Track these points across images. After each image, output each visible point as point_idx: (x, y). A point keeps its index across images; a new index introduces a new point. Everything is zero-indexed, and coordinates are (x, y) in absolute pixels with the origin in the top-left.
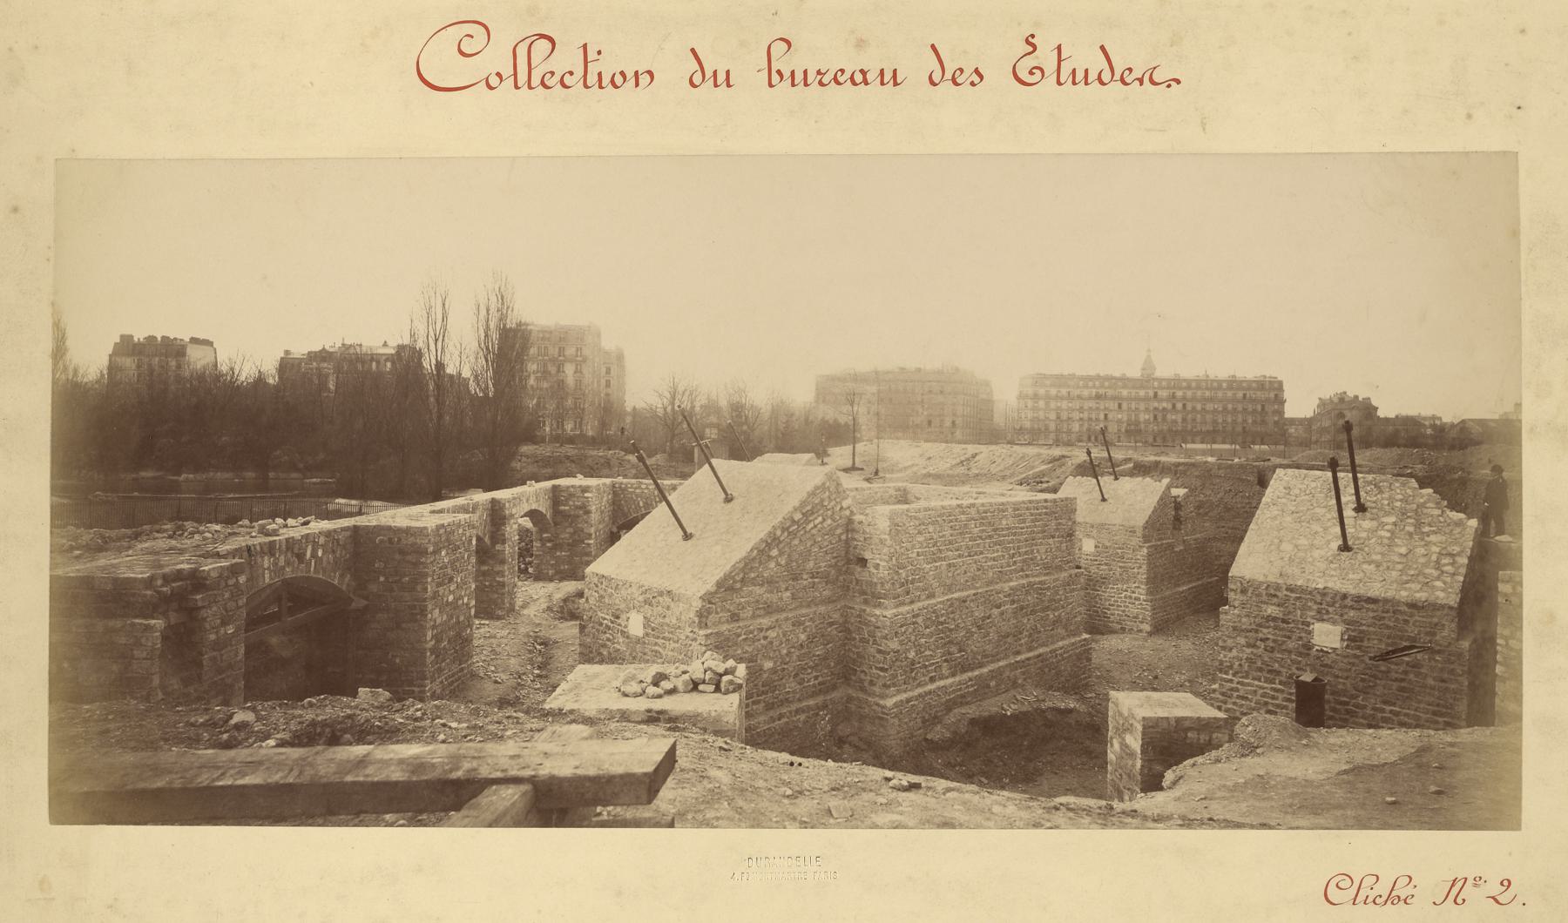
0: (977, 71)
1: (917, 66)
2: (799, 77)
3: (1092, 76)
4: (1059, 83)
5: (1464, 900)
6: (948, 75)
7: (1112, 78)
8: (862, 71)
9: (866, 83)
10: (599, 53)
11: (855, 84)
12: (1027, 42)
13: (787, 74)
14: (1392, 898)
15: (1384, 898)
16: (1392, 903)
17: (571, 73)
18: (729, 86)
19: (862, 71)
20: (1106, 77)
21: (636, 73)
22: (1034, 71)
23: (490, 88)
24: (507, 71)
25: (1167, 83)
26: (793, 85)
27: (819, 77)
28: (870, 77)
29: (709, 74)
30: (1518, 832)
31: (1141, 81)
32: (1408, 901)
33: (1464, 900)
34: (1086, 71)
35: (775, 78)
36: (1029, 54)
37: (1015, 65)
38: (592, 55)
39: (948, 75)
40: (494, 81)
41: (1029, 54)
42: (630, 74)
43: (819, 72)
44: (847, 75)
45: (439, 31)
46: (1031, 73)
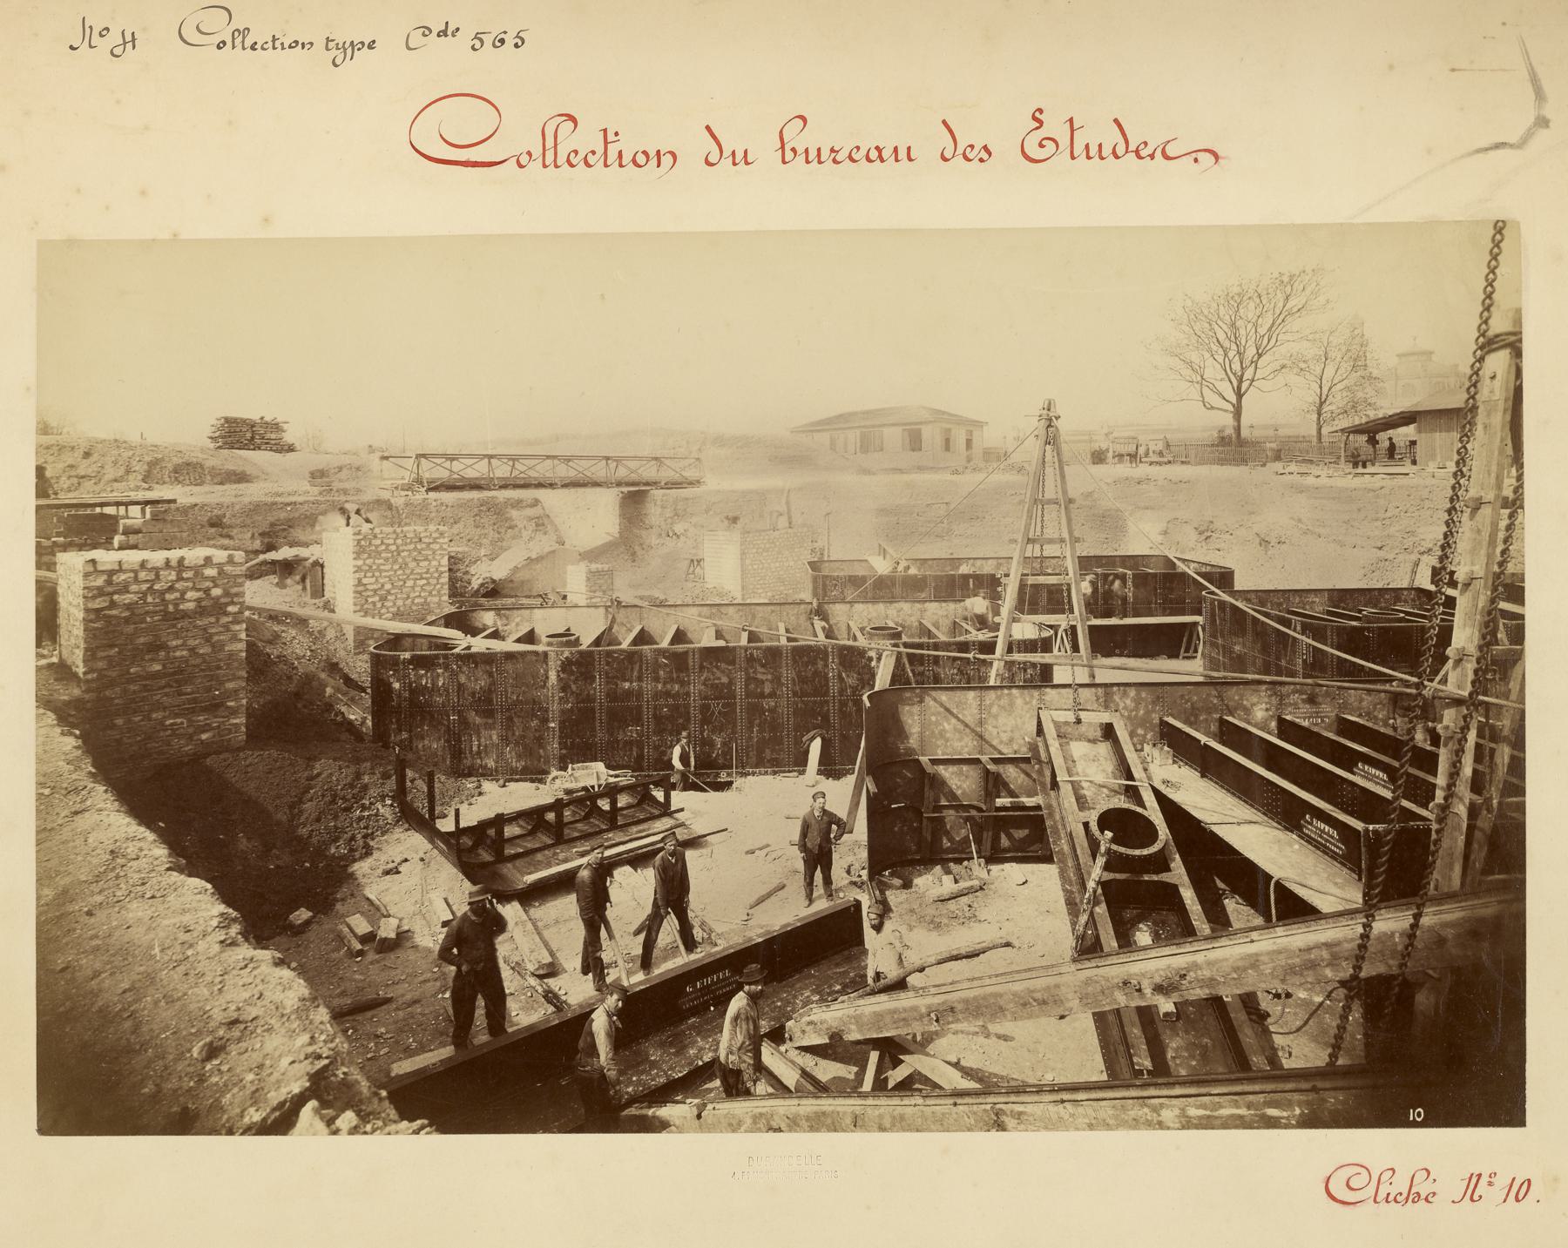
0: (985, 148)
1: (695, 145)
2: (813, 155)
3: (1106, 151)
4: (1073, 158)
5: (1481, 1197)
6: (960, 151)
7: (1127, 148)
8: (877, 148)
9: (882, 160)
10: (616, 134)
11: (869, 160)
12: (1034, 118)
13: (800, 150)
14: (1412, 1197)
15: (1405, 1195)
16: (1413, 1202)
17: (593, 153)
18: (910, 159)
19: (877, 148)
20: (1121, 150)
21: (658, 152)
22: (1044, 143)
23: (521, 166)
24: (537, 152)
25: (1194, 155)
26: (807, 162)
27: (833, 155)
28: (885, 154)
29: (727, 153)
30: (1523, 1129)
31: (1152, 156)
32: (1430, 1199)
33: (1481, 1197)
34: (1100, 146)
35: (789, 155)
36: (1037, 128)
37: (781, 132)
38: (611, 137)
39: (960, 151)
40: (524, 160)
41: (1037, 128)
42: (652, 154)
43: (832, 150)
44: (863, 152)
45: (434, 102)
46: (1041, 146)
